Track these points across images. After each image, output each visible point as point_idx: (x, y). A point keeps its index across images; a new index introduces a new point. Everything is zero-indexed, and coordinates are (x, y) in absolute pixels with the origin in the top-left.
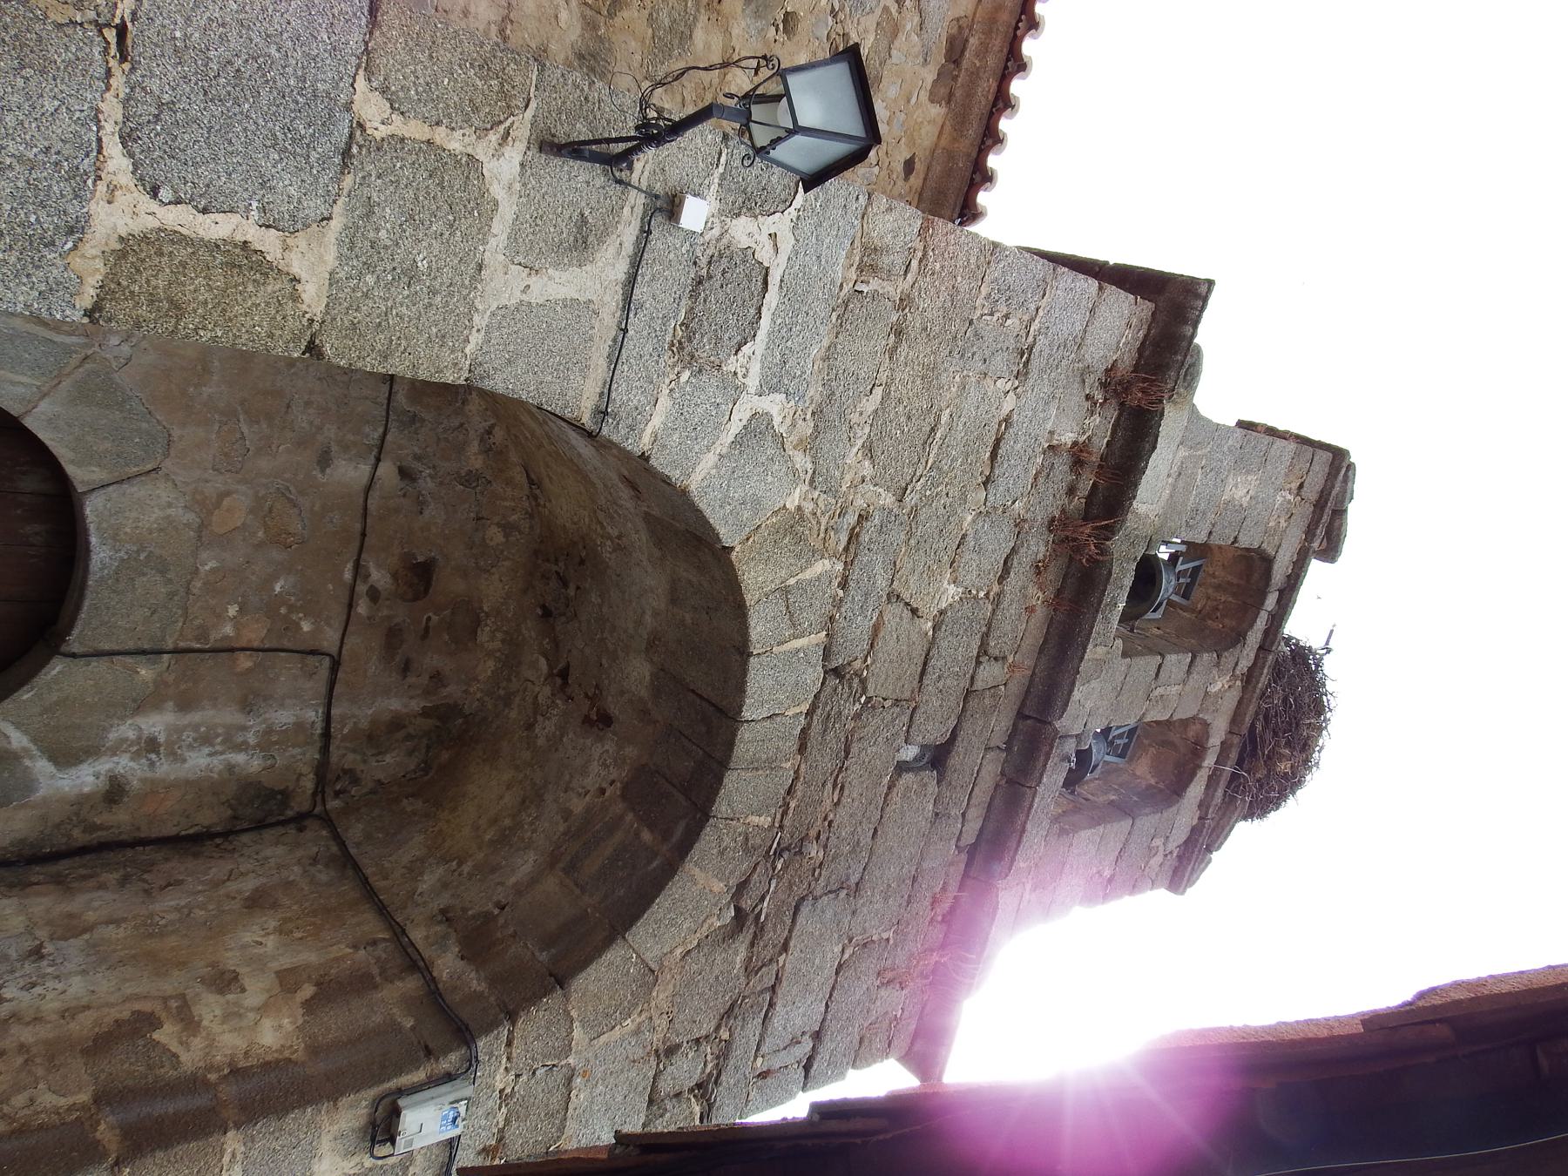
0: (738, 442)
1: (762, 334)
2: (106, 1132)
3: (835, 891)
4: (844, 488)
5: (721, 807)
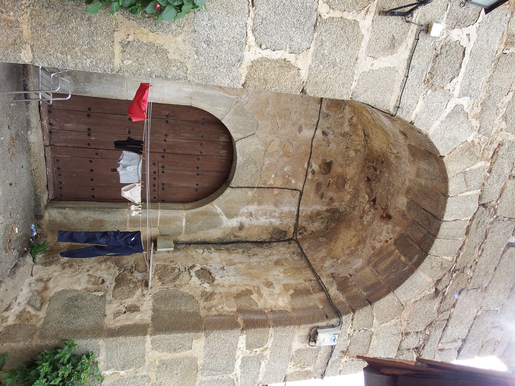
0: (449, 116)
1: (461, 74)
3: (476, 289)
4: (493, 133)
5: (433, 251)
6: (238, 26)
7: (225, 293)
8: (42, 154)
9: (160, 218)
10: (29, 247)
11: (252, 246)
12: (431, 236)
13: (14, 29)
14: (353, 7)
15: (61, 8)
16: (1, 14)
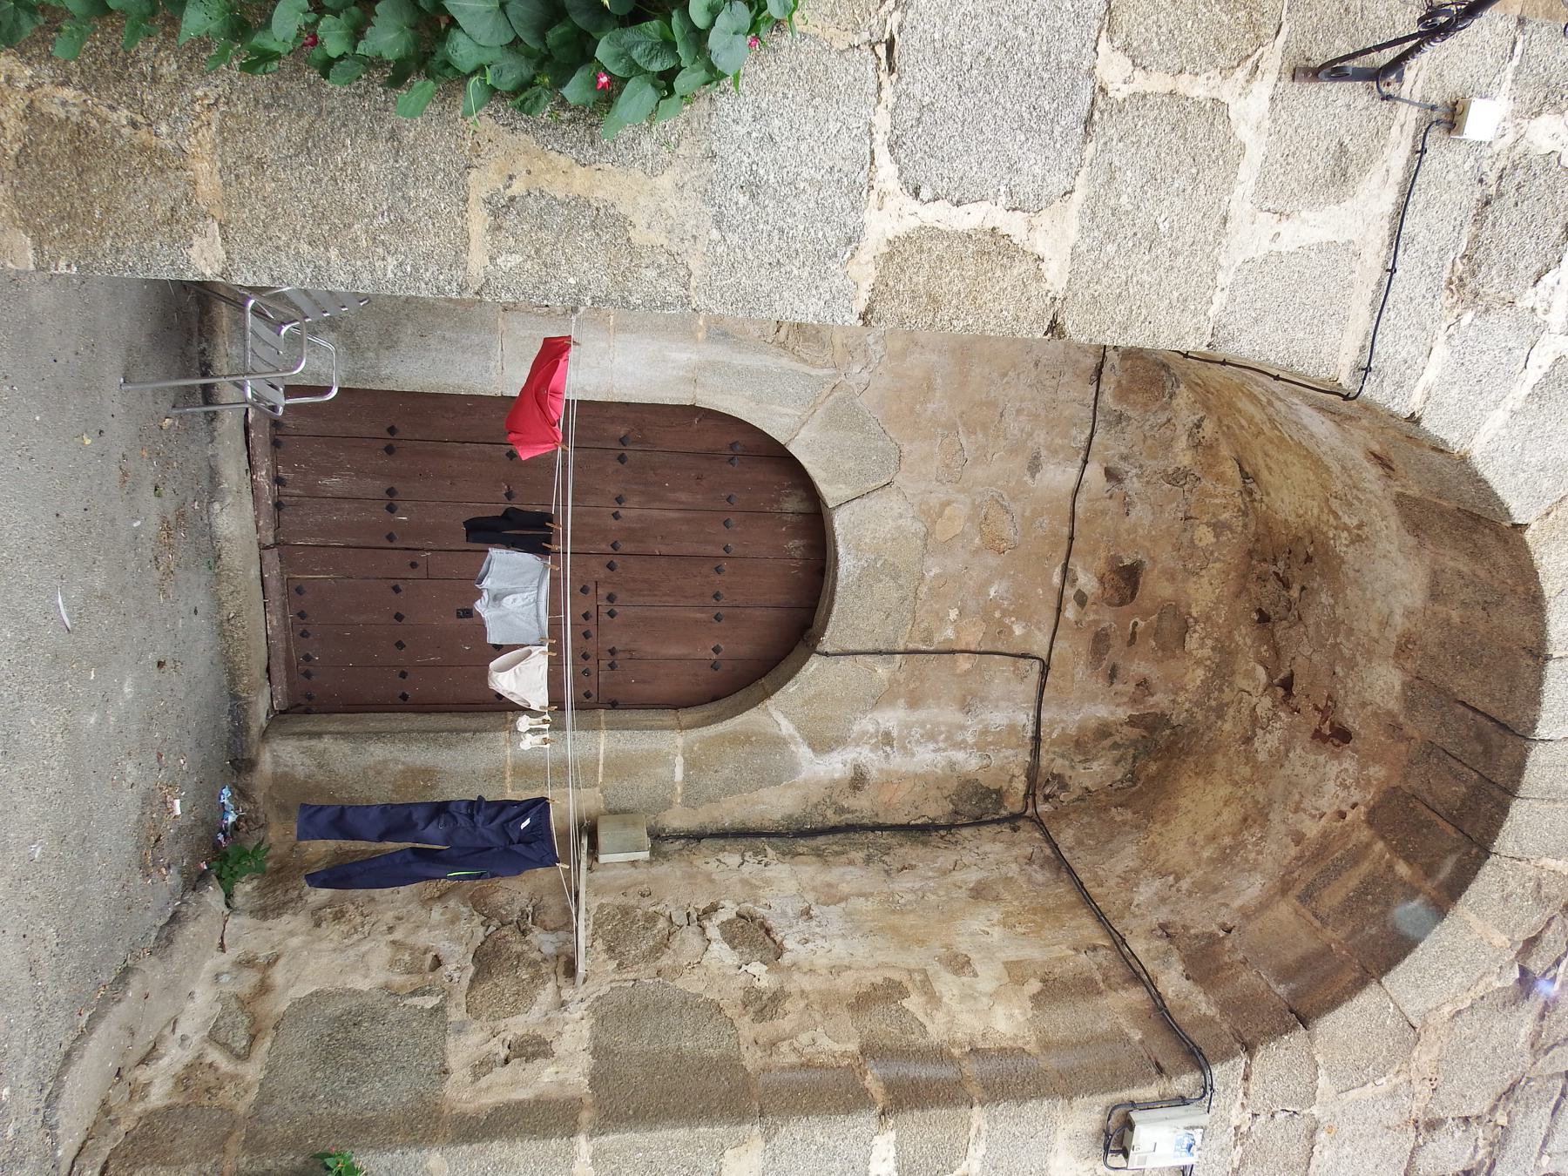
0: (1536, 394)
2: (872, 1081)
5: (1505, 842)
6: (845, 135)
7: (820, 992)
8: (254, 572)
9: (606, 757)
10: (214, 860)
11: (894, 841)
12: (1496, 793)
13: (172, 176)
14: (1210, 60)
15: (310, 106)
16: (133, 131)
